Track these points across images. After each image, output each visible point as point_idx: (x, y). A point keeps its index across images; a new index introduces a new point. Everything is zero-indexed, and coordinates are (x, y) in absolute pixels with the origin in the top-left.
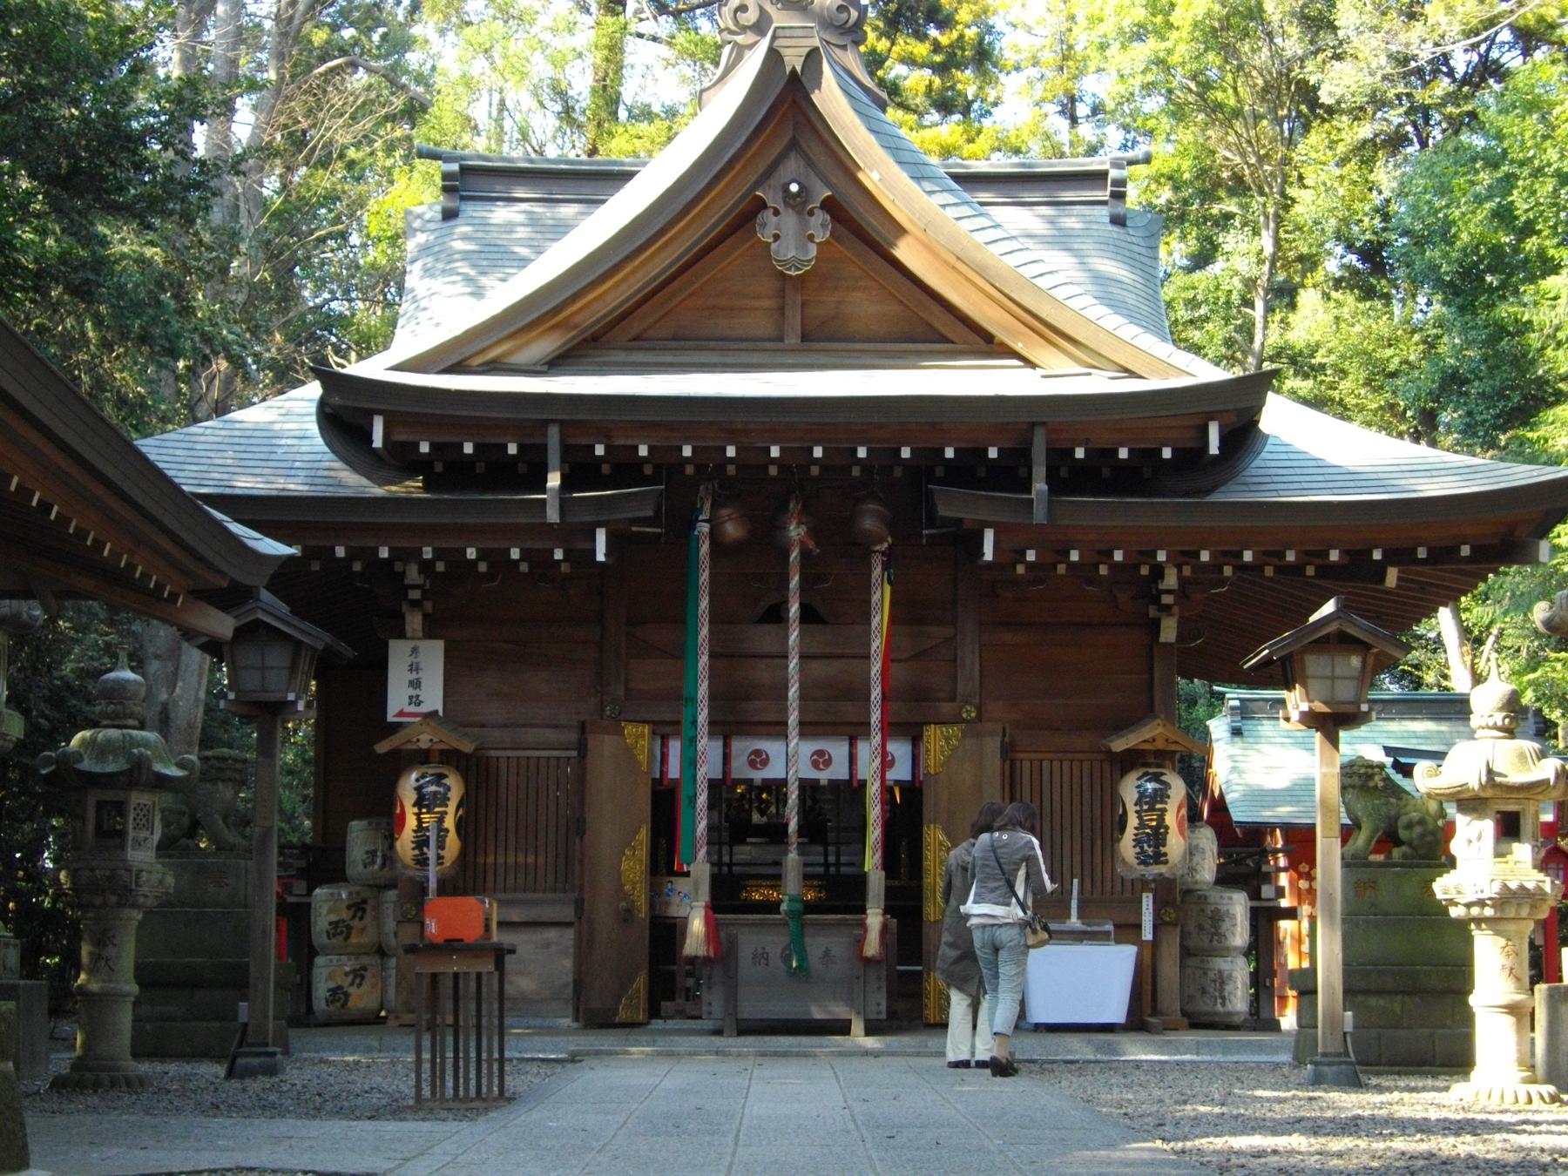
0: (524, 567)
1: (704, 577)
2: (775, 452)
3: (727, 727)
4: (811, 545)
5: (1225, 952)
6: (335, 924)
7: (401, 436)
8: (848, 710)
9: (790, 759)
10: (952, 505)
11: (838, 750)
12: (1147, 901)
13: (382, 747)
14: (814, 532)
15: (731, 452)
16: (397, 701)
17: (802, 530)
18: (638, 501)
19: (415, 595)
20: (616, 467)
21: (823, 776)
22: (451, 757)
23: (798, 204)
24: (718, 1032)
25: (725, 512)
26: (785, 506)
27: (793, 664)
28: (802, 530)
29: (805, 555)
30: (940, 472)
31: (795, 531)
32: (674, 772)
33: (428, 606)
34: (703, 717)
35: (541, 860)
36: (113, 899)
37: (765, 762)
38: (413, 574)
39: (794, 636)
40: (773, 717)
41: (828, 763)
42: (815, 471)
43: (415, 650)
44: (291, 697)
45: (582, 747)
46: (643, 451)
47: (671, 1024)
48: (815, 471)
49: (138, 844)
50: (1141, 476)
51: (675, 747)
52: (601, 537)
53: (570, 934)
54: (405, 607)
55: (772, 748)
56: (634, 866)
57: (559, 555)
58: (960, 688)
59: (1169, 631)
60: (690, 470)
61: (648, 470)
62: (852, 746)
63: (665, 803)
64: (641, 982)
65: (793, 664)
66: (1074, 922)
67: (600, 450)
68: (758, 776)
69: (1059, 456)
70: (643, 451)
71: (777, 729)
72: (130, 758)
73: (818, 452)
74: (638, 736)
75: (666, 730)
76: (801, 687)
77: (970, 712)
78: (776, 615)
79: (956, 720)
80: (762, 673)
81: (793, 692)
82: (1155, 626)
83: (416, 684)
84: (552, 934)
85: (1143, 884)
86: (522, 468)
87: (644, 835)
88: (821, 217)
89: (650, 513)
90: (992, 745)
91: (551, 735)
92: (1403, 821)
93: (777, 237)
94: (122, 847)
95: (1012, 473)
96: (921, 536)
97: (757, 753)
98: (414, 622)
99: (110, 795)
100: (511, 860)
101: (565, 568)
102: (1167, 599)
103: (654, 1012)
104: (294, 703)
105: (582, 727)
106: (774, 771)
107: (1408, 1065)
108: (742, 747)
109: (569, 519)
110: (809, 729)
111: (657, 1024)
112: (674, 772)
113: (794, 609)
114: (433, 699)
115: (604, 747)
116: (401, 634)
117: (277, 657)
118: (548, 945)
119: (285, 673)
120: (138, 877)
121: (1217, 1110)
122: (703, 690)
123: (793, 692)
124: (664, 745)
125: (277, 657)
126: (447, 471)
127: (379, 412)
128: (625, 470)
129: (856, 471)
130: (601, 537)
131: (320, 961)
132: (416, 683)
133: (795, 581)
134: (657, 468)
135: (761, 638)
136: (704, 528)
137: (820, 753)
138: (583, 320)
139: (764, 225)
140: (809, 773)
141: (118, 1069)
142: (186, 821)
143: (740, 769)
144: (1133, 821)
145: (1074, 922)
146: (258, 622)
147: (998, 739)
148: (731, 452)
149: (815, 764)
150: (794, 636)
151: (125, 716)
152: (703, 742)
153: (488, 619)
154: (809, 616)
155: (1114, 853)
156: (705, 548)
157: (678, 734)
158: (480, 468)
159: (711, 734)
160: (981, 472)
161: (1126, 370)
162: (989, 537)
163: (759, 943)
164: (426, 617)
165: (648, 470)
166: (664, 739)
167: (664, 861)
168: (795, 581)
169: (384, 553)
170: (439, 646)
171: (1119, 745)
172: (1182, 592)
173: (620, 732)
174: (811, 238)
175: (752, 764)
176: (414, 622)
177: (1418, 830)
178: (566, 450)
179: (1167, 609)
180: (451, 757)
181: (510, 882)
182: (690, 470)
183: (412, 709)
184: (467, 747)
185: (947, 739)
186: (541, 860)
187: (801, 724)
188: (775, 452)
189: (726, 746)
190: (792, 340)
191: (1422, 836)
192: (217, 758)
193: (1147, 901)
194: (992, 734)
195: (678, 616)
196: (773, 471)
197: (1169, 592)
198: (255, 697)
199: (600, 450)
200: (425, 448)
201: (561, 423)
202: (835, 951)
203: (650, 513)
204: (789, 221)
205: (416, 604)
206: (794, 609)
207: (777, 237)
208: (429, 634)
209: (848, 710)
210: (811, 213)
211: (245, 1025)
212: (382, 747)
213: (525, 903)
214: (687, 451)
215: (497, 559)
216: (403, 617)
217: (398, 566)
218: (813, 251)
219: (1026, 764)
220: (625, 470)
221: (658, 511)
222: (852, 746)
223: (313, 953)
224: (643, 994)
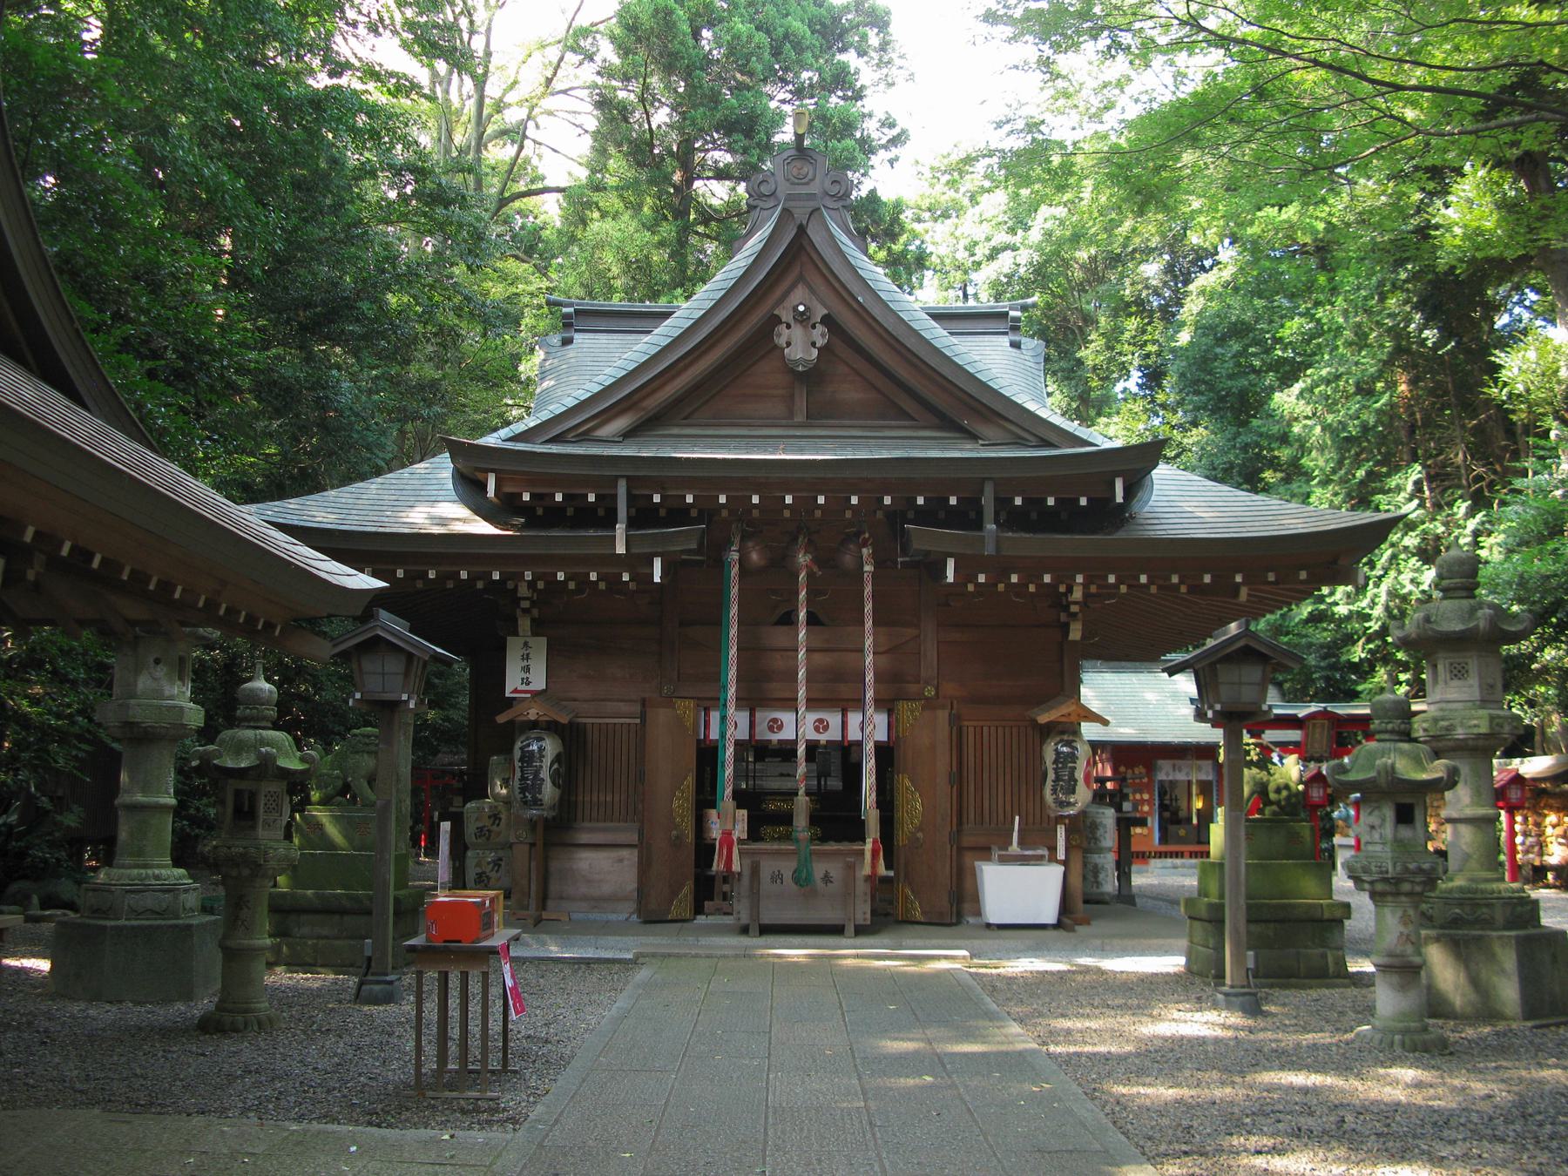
0: (602, 586)
1: (734, 591)
2: (789, 500)
3: (752, 700)
4: (815, 569)
5: (1100, 851)
6: (481, 829)
7: (509, 489)
8: (845, 690)
9: (799, 725)
10: (923, 538)
11: (834, 719)
12: (1061, 832)
13: (501, 719)
14: (815, 560)
15: (755, 500)
16: (513, 682)
17: (808, 558)
18: (684, 539)
19: (525, 604)
20: (670, 511)
21: (823, 738)
22: (552, 727)
23: (803, 319)
24: (745, 930)
25: (750, 544)
26: (795, 539)
27: (802, 654)
28: (808, 558)
29: (810, 575)
30: (911, 515)
31: (803, 559)
32: (714, 734)
33: (535, 612)
34: (732, 691)
35: (617, 798)
36: (246, 872)
37: (780, 728)
38: (523, 591)
39: (802, 634)
40: (787, 695)
41: (826, 728)
42: (818, 513)
43: (526, 644)
44: (405, 697)
45: (643, 716)
46: (689, 499)
47: (712, 920)
48: (818, 513)
49: (267, 824)
50: (1067, 519)
51: (715, 716)
52: (657, 563)
53: (635, 852)
54: (519, 612)
55: (787, 718)
56: (682, 804)
57: (626, 577)
58: (923, 674)
59: (1075, 634)
60: (725, 513)
61: (694, 513)
62: (844, 716)
63: (708, 755)
64: (687, 889)
65: (802, 654)
66: (1014, 848)
67: (657, 499)
68: (775, 737)
69: (1003, 502)
70: (689, 499)
71: (790, 703)
72: (260, 755)
73: (821, 500)
74: (685, 708)
75: (707, 703)
76: (808, 671)
77: (930, 692)
78: (788, 620)
79: (918, 697)
80: (778, 662)
81: (802, 673)
82: (1065, 628)
83: (527, 669)
84: (625, 853)
85: (1060, 819)
86: (601, 512)
87: (690, 781)
88: (820, 329)
89: (694, 546)
90: (943, 716)
91: (624, 708)
92: (1272, 787)
93: (789, 344)
94: (254, 828)
95: (968, 518)
96: (896, 562)
97: (775, 720)
98: (524, 624)
99: (244, 785)
100: (595, 799)
101: (632, 586)
102: (1074, 609)
103: (699, 910)
104: (407, 702)
105: (644, 702)
106: (787, 734)
107: (1279, 977)
108: (764, 716)
109: (634, 551)
110: (813, 703)
111: (701, 919)
112: (714, 734)
113: (802, 615)
114: (539, 682)
115: (661, 717)
116: (516, 634)
117: (394, 665)
118: (621, 860)
119: (401, 678)
120: (266, 853)
121: (1193, 1092)
122: (732, 673)
123: (802, 673)
124: (707, 715)
125: (394, 665)
126: (541, 516)
127: (492, 471)
128: (678, 514)
129: (848, 514)
130: (657, 563)
131: (469, 853)
132: (527, 673)
133: (803, 594)
134: (701, 512)
135: (778, 636)
136: (735, 556)
137: (820, 721)
138: (647, 402)
139: (779, 335)
140: (812, 735)
141: (253, 1011)
142: (340, 783)
143: (763, 734)
144: (1051, 776)
145: (1014, 848)
146: (378, 636)
147: (946, 713)
148: (755, 500)
149: (817, 729)
150: (802, 634)
151: (257, 719)
152: (731, 710)
153: (576, 628)
154: (812, 620)
155: (1042, 798)
156: (735, 571)
157: (716, 707)
158: (662, 512)
159: (738, 708)
160: (942, 515)
161: (1042, 440)
162: (951, 564)
163: (778, 864)
164: (533, 620)
165: (694, 513)
166: (707, 710)
167: (705, 798)
168: (803, 594)
169: (496, 576)
170: (544, 640)
171: (1043, 719)
172: (1084, 604)
173: (672, 706)
174: (814, 344)
175: (771, 729)
176: (524, 624)
177: (1285, 793)
178: (631, 499)
179: (1074, 615)
180: (552, 727)
181: (594, 814)
182: (725, 513)
183: (524, 687)
184: (564, 720)
185: (912, 712)
186: (617, 798)
187: (808, 700)
188: (789, 500)
189: (752, 716)
190: (800, 418)
191: (1288, 798)
192: (364, 736)
193: (1061, 832)
194: (943, 707)
195: (717, 621)
196: (787, 513)
197: (1076, 603)
198: (377, 697)
199: (657, 499)
200: (526, 497)
201: (628, 478)
202: (833, 873)
203: (694, 546)
204: (797, 333)
205: (526, 611)
206: (802, 615)
207: (789, 344)
208: (535, 633)
209: (845, 690)
210: (814, 327)
211: (369, 959)
212: (501, 719)
213: (605, 830)
214: (722, 499)
215: (583, 581)
216: (516, 620)
217: (510, 585)
218: (815, 353)
219: (971, 730)
220: (678, 514)
221: (701, 544)
222: (844, 716)
223: (466, 848)
224: (690, 898)
